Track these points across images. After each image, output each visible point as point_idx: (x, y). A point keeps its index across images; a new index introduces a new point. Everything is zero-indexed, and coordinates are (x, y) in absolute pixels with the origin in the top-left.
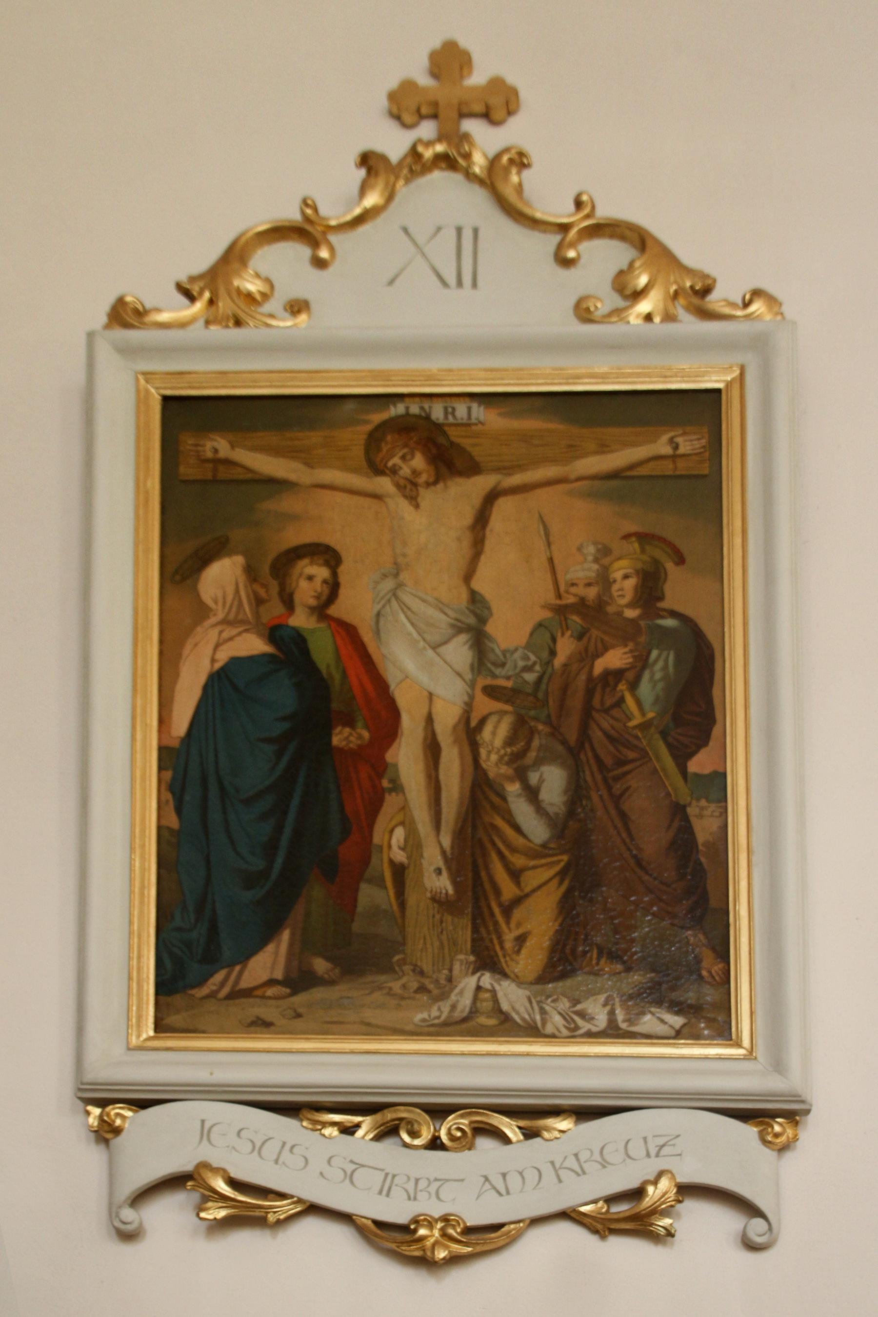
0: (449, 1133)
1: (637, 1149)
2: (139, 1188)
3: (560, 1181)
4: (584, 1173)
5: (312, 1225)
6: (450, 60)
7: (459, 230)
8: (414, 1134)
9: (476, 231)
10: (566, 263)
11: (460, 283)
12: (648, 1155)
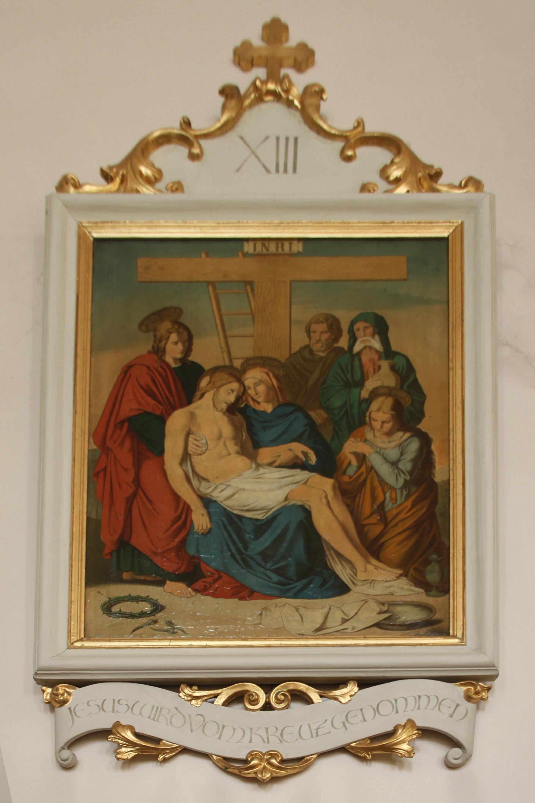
2: (71, 740)
5: (184, 760)
6: (275, 30)
7: (278, 139)
9: (296, 140)
10: (349, 159)
11: (277, 170)
12: (312, 737)
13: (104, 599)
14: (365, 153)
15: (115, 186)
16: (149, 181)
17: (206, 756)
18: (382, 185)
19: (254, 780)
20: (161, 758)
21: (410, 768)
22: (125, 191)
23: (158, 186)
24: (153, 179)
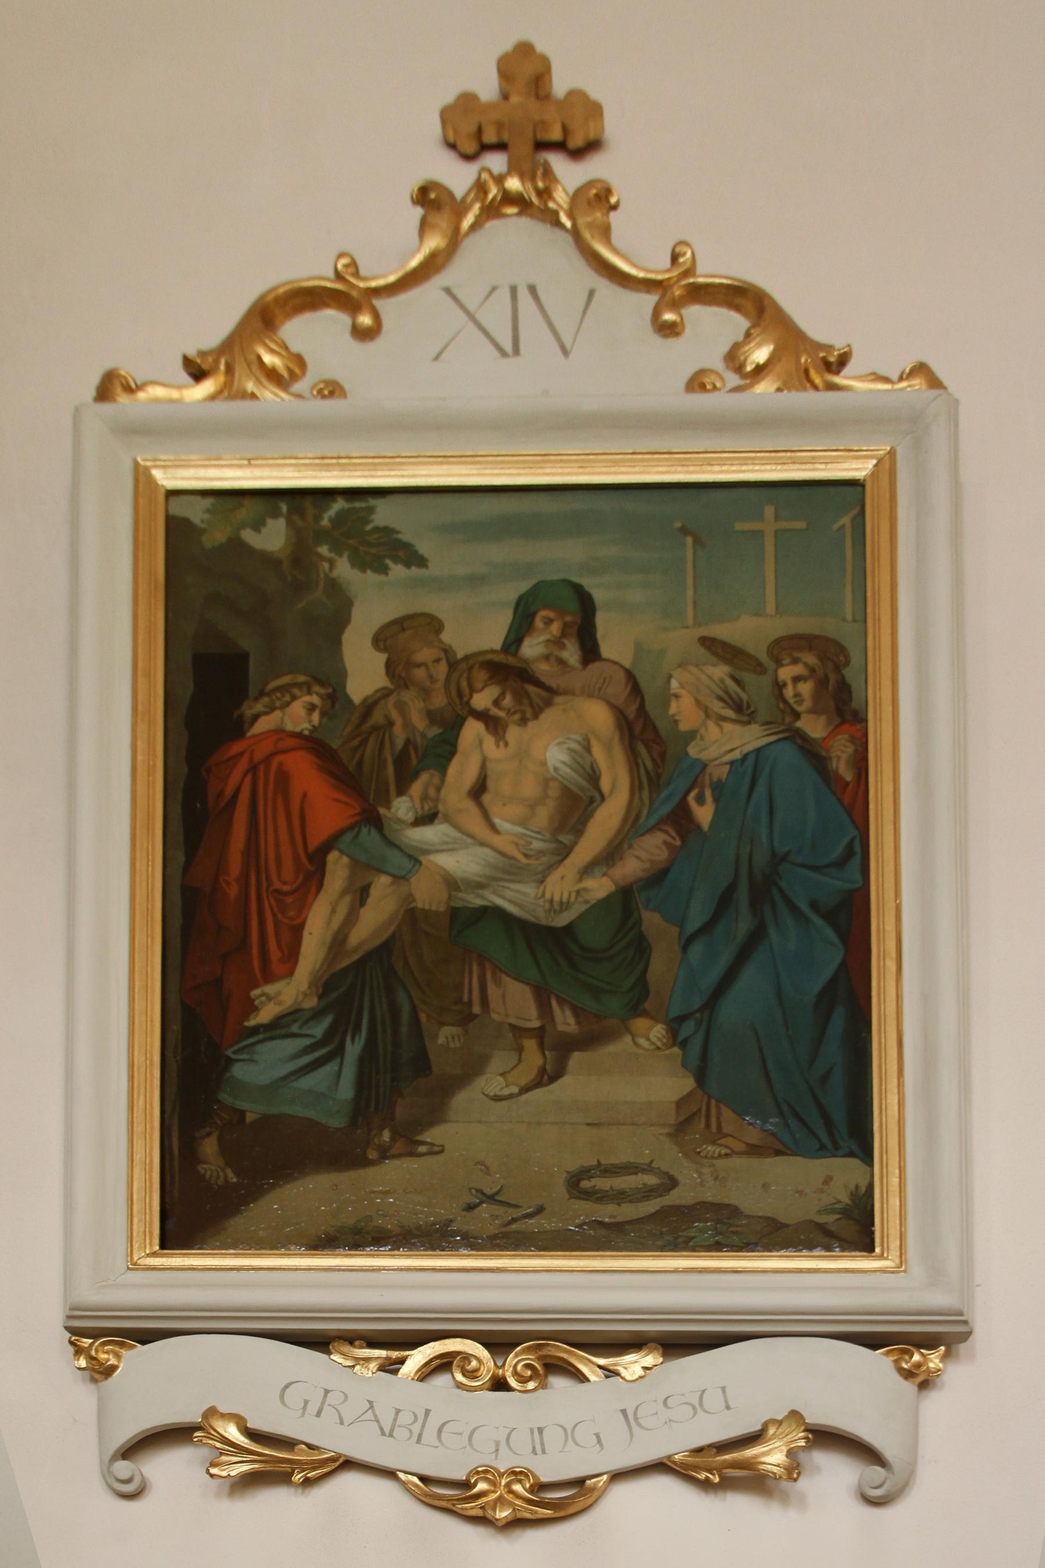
0: (515, 1373)
1: (713, 1400)
3: (598, 1436)
4: (391, 1435)
8: (472, 1375)
13: (674, 1192)
14: (697, 315)
15: (208, 386)
16: (272, 375)
17: (390, 1474)
18: (733, 380)
19: (481, 1520)
20: (298, 1477)
21: (802, 1503)
22: (232, 397)
23: (298, 387)
24: (285, 374)
